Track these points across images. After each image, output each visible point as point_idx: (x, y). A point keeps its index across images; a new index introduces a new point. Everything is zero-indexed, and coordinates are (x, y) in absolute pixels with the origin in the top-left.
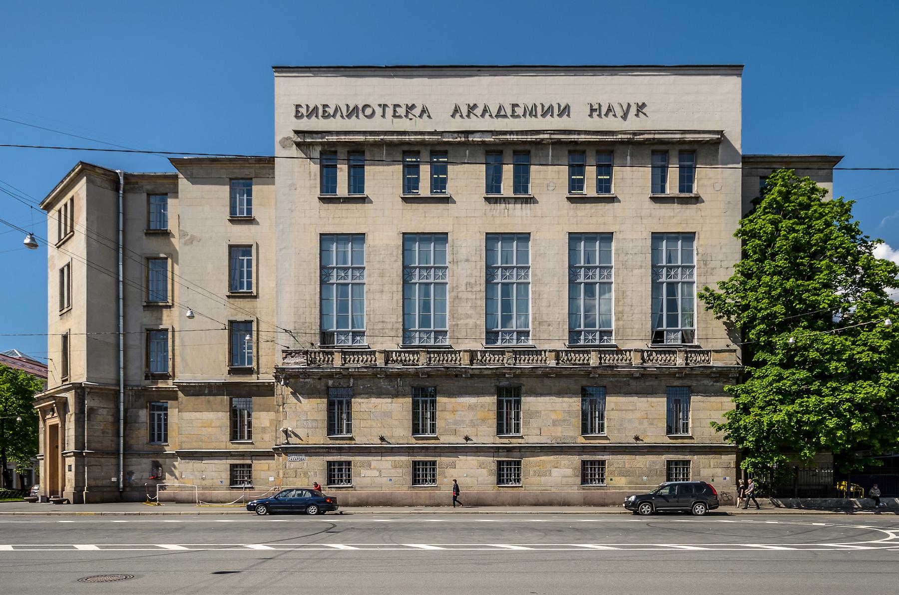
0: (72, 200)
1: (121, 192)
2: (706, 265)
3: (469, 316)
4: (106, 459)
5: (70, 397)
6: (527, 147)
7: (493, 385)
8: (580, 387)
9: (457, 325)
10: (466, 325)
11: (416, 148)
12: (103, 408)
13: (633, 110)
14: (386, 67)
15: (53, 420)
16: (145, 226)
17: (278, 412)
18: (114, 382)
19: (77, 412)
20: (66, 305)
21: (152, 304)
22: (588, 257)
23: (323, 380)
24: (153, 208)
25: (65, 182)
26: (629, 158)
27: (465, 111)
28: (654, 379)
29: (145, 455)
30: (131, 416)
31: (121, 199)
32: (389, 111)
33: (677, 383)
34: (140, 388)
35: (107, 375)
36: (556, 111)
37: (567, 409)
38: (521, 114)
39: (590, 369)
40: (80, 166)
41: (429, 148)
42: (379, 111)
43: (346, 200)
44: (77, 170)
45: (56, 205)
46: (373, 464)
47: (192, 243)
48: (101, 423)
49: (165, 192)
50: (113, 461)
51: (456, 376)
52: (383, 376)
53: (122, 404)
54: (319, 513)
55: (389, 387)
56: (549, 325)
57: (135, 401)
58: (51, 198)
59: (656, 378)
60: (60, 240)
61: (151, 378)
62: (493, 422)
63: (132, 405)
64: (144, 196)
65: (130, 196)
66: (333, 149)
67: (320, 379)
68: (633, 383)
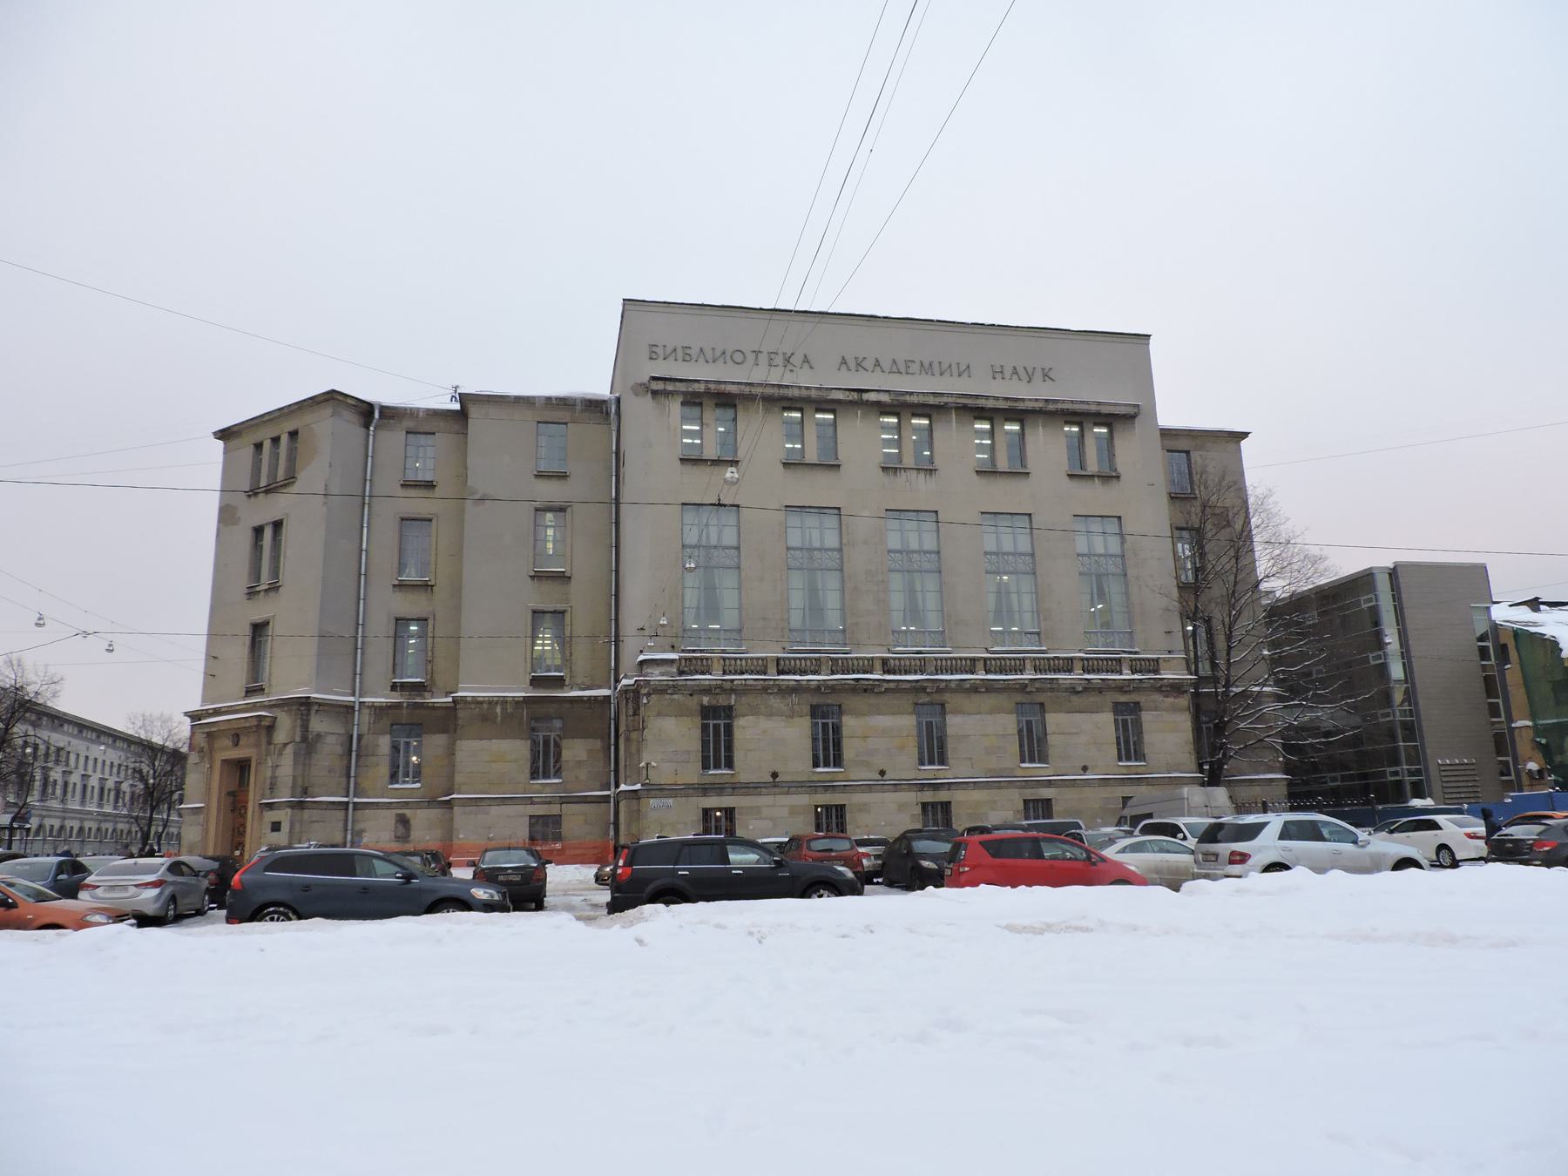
1: (372, 428)
7: (910, 702)
26: (1040, 428)
28: (1097, 693)
31: (371, 437)
37: (1001, 733)
42: (750, 357)
53: (356, 727)
57: (374, 722)
65: (383, 435)
66: (697, 401)
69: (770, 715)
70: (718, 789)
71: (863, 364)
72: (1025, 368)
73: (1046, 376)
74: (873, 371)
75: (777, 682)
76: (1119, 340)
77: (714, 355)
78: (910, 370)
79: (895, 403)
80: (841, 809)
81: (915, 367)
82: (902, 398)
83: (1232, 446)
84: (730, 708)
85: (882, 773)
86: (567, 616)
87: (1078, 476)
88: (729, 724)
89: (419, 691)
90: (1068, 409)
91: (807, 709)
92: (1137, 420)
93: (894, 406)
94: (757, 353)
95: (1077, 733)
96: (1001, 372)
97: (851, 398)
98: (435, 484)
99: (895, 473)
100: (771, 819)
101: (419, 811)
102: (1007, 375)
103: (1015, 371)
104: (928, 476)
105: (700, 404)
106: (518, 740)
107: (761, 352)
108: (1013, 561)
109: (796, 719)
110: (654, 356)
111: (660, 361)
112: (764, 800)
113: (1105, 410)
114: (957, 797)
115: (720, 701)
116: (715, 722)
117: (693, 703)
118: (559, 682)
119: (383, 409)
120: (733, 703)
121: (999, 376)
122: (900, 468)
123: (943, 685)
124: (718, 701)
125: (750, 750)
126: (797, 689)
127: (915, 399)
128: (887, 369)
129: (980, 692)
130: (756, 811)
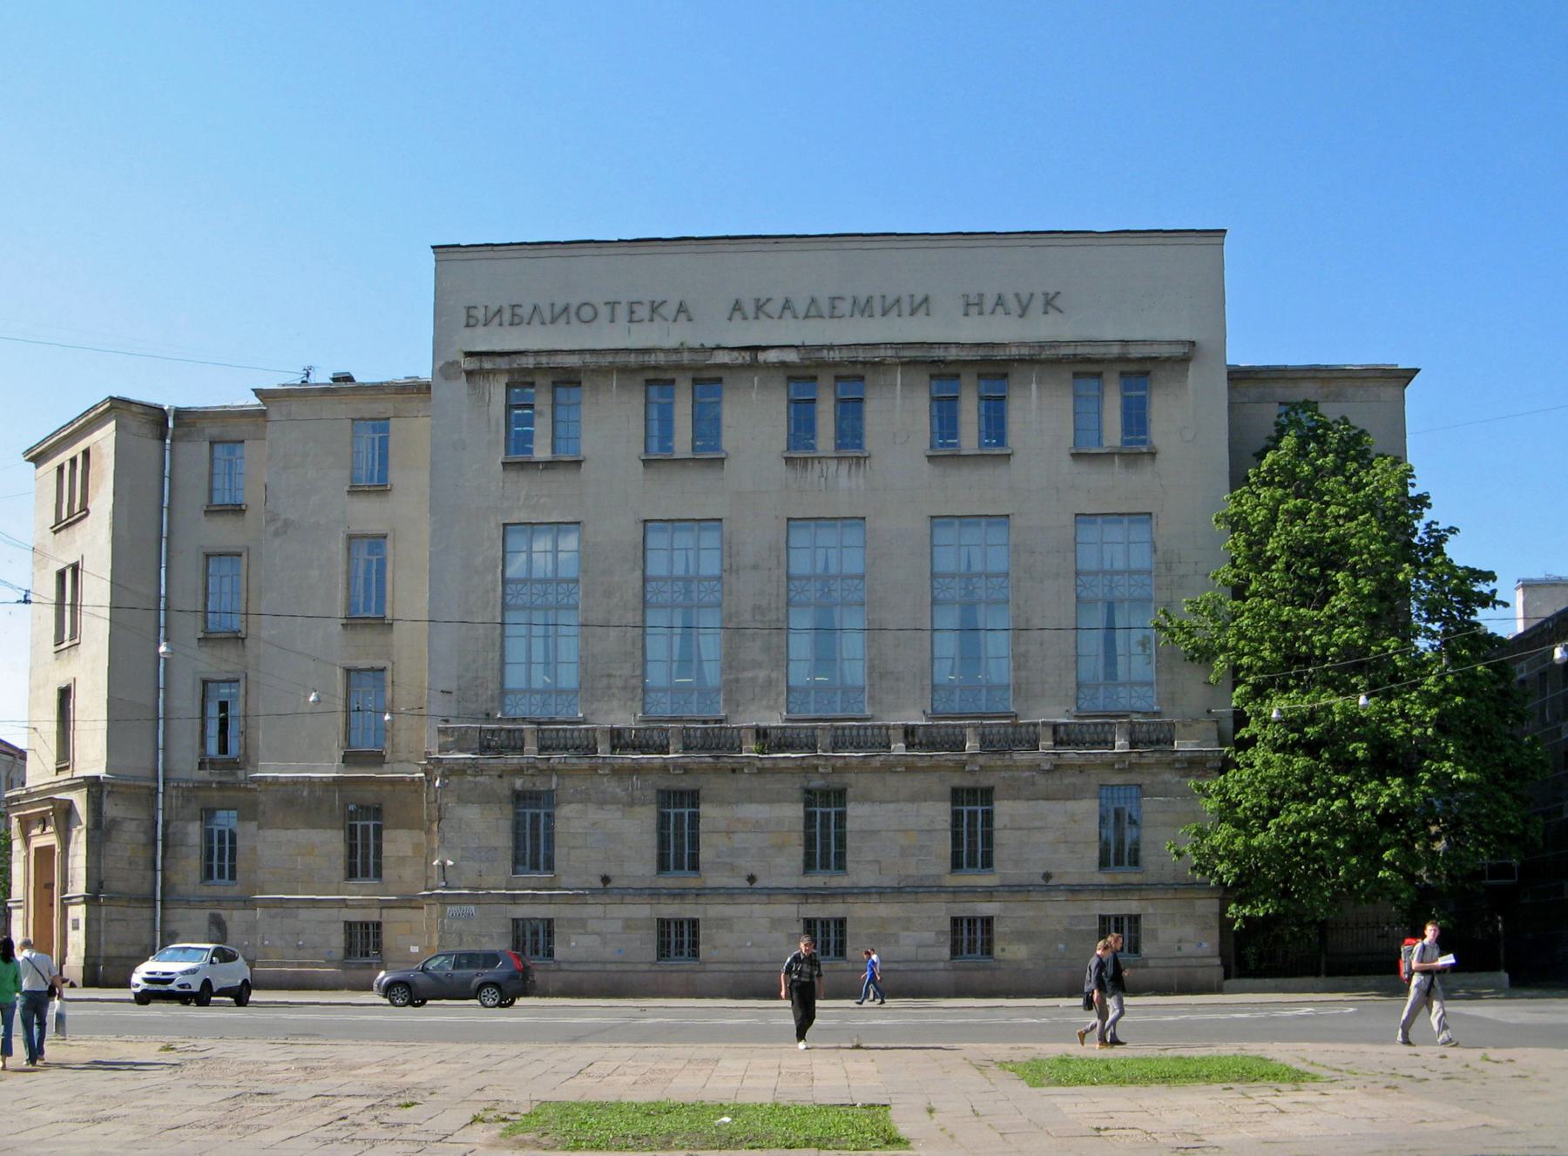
0: (86, 453)
1: (168, 441)
2: (1169, 569)
3: (758, 665)
4: (137, 910)
5: (79, 800)
6: (859, 370)
7: (798, 786)
8: (949, 790)
9: (737, 680)
10: (753, 679)
11: (668, 376)
12: (132, 819)
13: (1038, 303)
14: (620, 241)
15: (45, 838)
16: (206, 500)
17: (429, 832)
18: (149, 774)
19: (90, 827)
20: (67, 636)
21: (213, 636)
22: (969, 562)
23: (506, 779)
24: (220, 466)
25: (77, 425)
26: (1034, 386)
27: (749, 308)
29: (200, 903)
30: (174, 834)
32: (622, 311)
33: (1117, 779)
34: (191, 785)
35: (137, 764)
36: (906, 308)
38: (848, 313)
39: (964, 758)
40: (108, 405)
41: (690, 375)
42: (604, 312)
43: (549, 465)
44: (101, 409)
45: (52, 458)
46: (592, 925)
47: (285, 532)
48: (128, 847)
49: (241, 439)
50: (147, 913)
51: (734, 771)
52: (607, 772)
53: (160, 812)
54: (500, 1005)
55: (618, 790)
56: (897, 679)
57: (182, 807)
58: (46, 445)
59: (1081, 772)
60: (58, 520)
61: (208, 766)
62: (798, 852)
63: (177, 814)
64: (207, 444)
65: (182, 447)
66: (529, 379)
67: (500, 776)
68: (1041, 781)
69: (602, 803)
70: (826, 895)
71: (1057, 302)
72: (1017, 295)
73: (1050, 303)
74: (780, 317)
75: (608, 761)
76: (757, 247)
77: (883, 306)
78: (837, 313)
79: (807, 362)
80: (694, 926)
81: (844, 307)
82: (818, 355)
83: (1388, 392)
84: (550, 792)
85: (752, 879)
86: (388, 675)
87: (519, 462)
88: (694, 813)
89: (231, 769)
90: (1075, 355)
91: (651, 794)
92: (1191, 365)
93: (807, 367)
94: (612, 305)
95: (1041, 828)
96: (968, 305)
97: (740, 361)
98: (244, 507)
99: (805, 467)
100: (599, 934)
101: (235, 912)
102: (988, 307)
103: (1000, 301)
104: (853, 467)
105: (1099, 375)
106: (329, 831)
107: (619, 303)
108: (534, 597)
109: (637, 809)
110: (472, 321)
111: (480, 330)
112: (591, 911)
113: (1135, 352)
114: (858, 912)
115: (538, 784)
116: (823, 810)
117: (503, 788)
118: (377, 759)
119: (180, 414)
120: (554, 787)
121: (974, 310)
122: (812, 458)
123: (839, 763)
124: (534, 784)
125: (573, 848)
126: (637, 770)
127: (836, 355)
128: (801, 314)
129: (896, 772)
130: (580, 924)
